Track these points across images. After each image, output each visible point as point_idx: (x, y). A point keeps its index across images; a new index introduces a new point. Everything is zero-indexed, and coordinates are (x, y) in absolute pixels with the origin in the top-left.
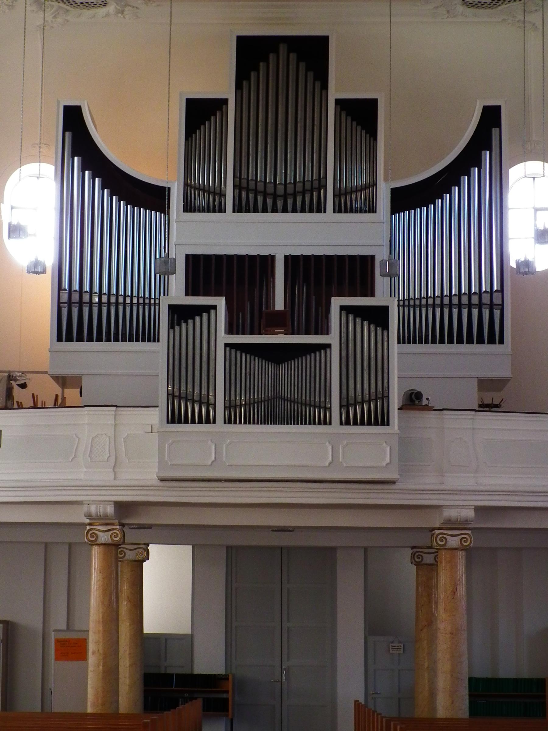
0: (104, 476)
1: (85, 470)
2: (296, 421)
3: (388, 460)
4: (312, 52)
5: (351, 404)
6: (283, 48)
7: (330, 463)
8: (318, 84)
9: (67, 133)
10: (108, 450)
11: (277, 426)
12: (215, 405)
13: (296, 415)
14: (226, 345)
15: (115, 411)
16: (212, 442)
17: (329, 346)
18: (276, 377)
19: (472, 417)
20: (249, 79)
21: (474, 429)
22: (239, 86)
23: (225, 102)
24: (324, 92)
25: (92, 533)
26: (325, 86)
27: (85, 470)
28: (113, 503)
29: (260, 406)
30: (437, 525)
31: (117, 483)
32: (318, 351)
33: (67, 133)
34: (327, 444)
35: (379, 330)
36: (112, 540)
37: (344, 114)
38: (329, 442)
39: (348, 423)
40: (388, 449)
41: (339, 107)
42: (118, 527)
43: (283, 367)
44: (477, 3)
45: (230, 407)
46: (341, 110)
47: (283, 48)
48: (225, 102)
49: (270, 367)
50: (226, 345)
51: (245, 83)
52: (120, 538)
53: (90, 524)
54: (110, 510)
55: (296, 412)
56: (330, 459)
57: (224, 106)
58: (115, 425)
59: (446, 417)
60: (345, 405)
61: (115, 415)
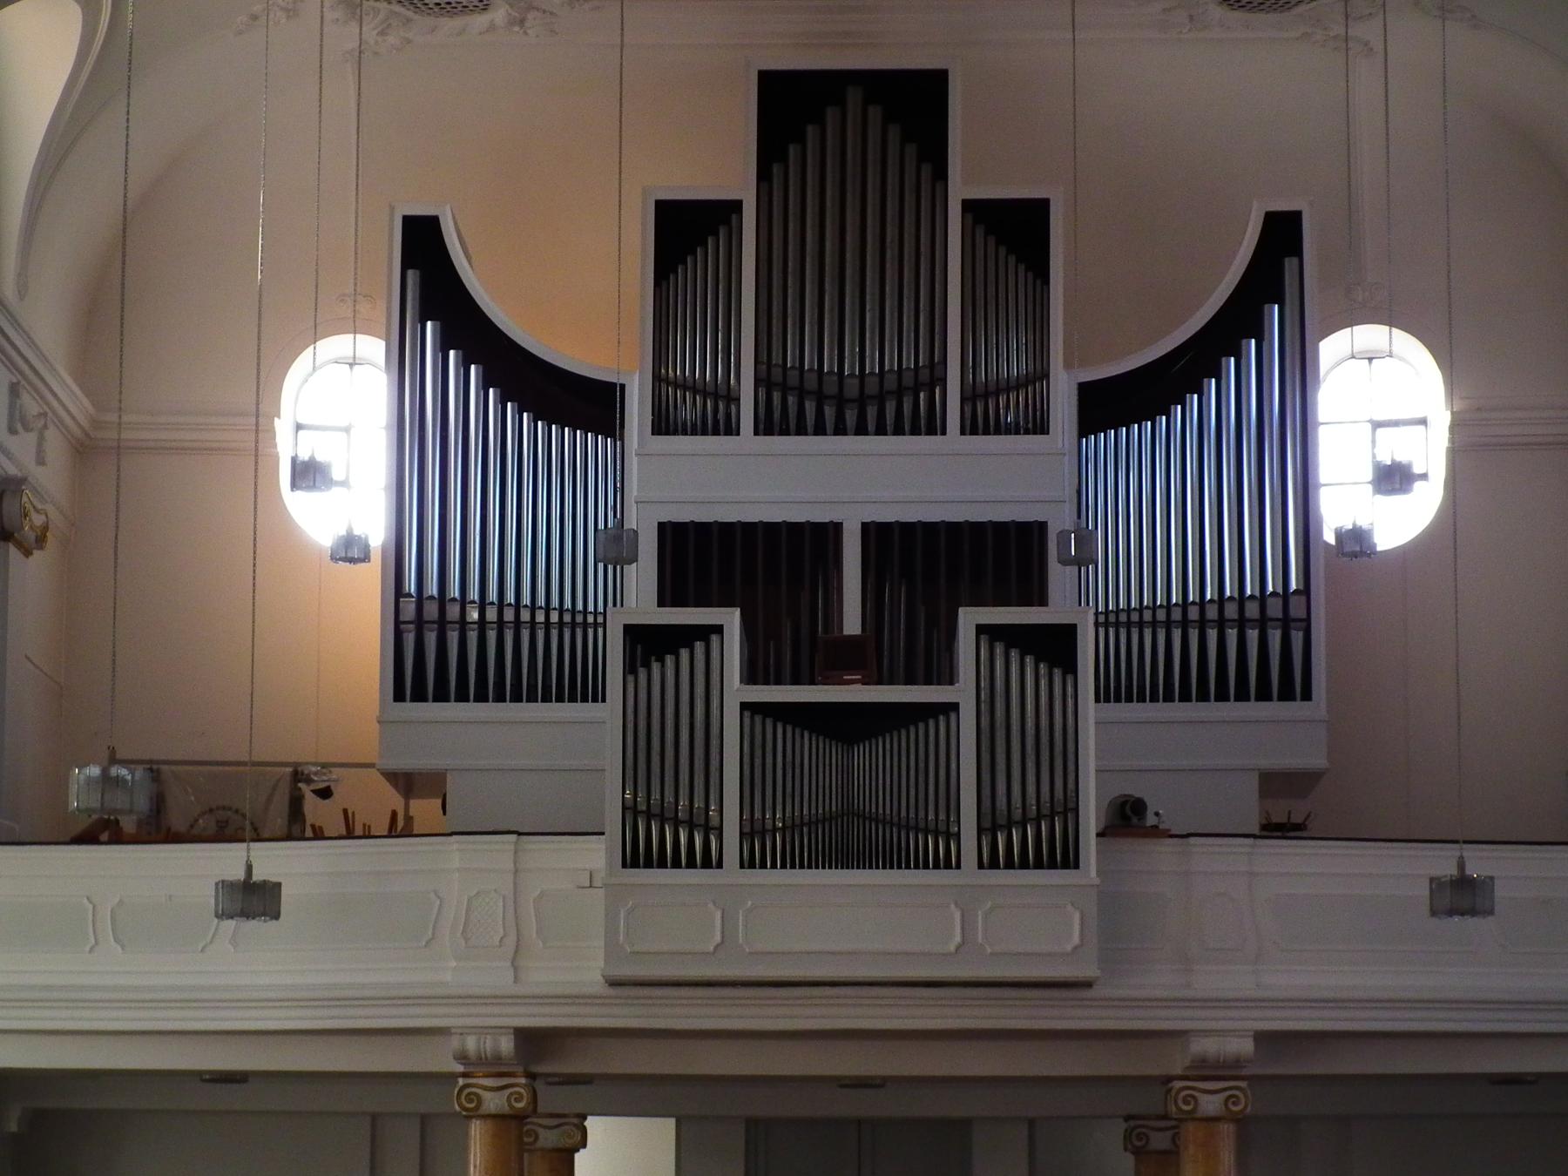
0: (494, 976)
6: (854, 97)
8: (926, 170)
9: (410, 273)
14: (744, 706)
17: (955, 707)
20: (784, 160)
22: (763, 175)
23: (736, 206)
24: (939, 186)
26: (941, 174)
37: (980, 232)
41: (969, 217)
42: (523, 1081)
46: (976, 222)
47: (854, 97)
48: (736, 206)
49: (833, 753)
51: (776, 169)
53: (465, 1075)
54: (507, 1045)
56: (958, 939)
57: (734, 216)
58: (516, 871)
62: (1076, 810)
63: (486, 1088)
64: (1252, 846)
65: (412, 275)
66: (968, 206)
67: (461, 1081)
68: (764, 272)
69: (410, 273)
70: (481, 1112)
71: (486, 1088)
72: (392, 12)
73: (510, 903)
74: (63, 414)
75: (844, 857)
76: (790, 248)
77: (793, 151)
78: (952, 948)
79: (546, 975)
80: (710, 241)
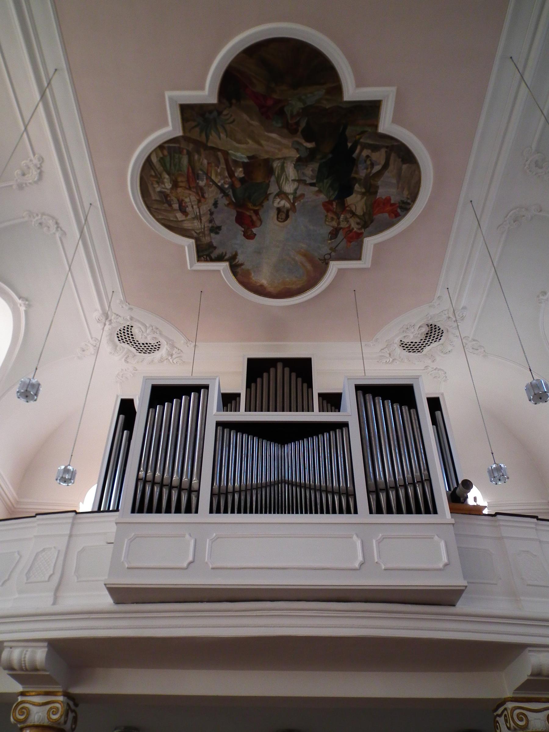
0: (42, 602)
1: (17, 596)
2: (308, 510)
3: (445, 560)
4: (302, 368)
5: (381, 490)
6: (280, 366)
7: (362, 564)
8: (305, 385)
9: (121, 416)
10: (53, 565)
11: (283, 515)
12: (198, 491)
13: (308, 503)
14: (218, 424)
15: (74, 518)
16: (190, 535)
17: (345, 425)
18: (281, 459)
19: (533, 526)
20: (256, 382)
21: (540, 541)
22: (248, 386)
23: (239, 395)
24: (310, 390)
25: (23, 708)
26: (310, 386)
27: (17, 596)
28: (46, 644)
29: (259, 492)
30: (509, 694)
31: (59, 608)
32: (333, 430)
33: (121, 416)
34: (355, 537)
35: (405, 409)
36: (49, 718)
37: (325, 402)
38: (357, 536)
39: (379, 511)
40: (442, 544)
41: (321, 398)
42: (61, 698)
43: (289, 449)
44: (410, 343)
45: (219, 495)
46: (323, 400)
47: (280, 366)
48: (239, 395)
49: (274, 448)
50: (218, 424)
51: (253, 385)
52: (61, 716)
53: (22, 694)
54: (40, 655)
55: (308, 500)
56: (360, 558)
57: (238, 398)
58: (70, 536)
59: (501, 523)
60: (374, 490)
61: (73, 524)
62: (430, 480)
63: (34, 704)
64: (536, 524)
65: (121, 416)
66: (320, 395)
67: (20, 699)
68: (249, 394)
69: (121, 416)
70: (28, 723)
71: (34, 704)
72: (129, 350)
73: (61, 558)
74: (4, 495)
75: (278, 507)
76: (258, 402)
77: (259, 380)
78: (357, 565)
79: (72, 601)
80: (229, 405)
